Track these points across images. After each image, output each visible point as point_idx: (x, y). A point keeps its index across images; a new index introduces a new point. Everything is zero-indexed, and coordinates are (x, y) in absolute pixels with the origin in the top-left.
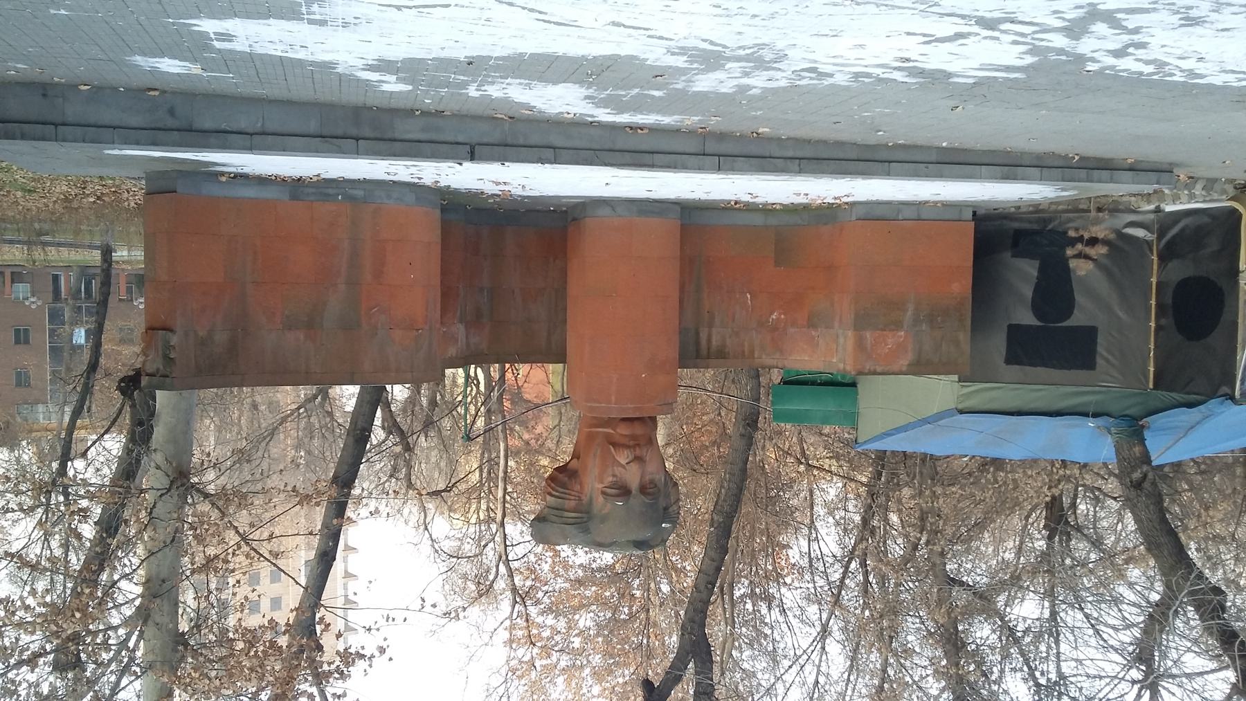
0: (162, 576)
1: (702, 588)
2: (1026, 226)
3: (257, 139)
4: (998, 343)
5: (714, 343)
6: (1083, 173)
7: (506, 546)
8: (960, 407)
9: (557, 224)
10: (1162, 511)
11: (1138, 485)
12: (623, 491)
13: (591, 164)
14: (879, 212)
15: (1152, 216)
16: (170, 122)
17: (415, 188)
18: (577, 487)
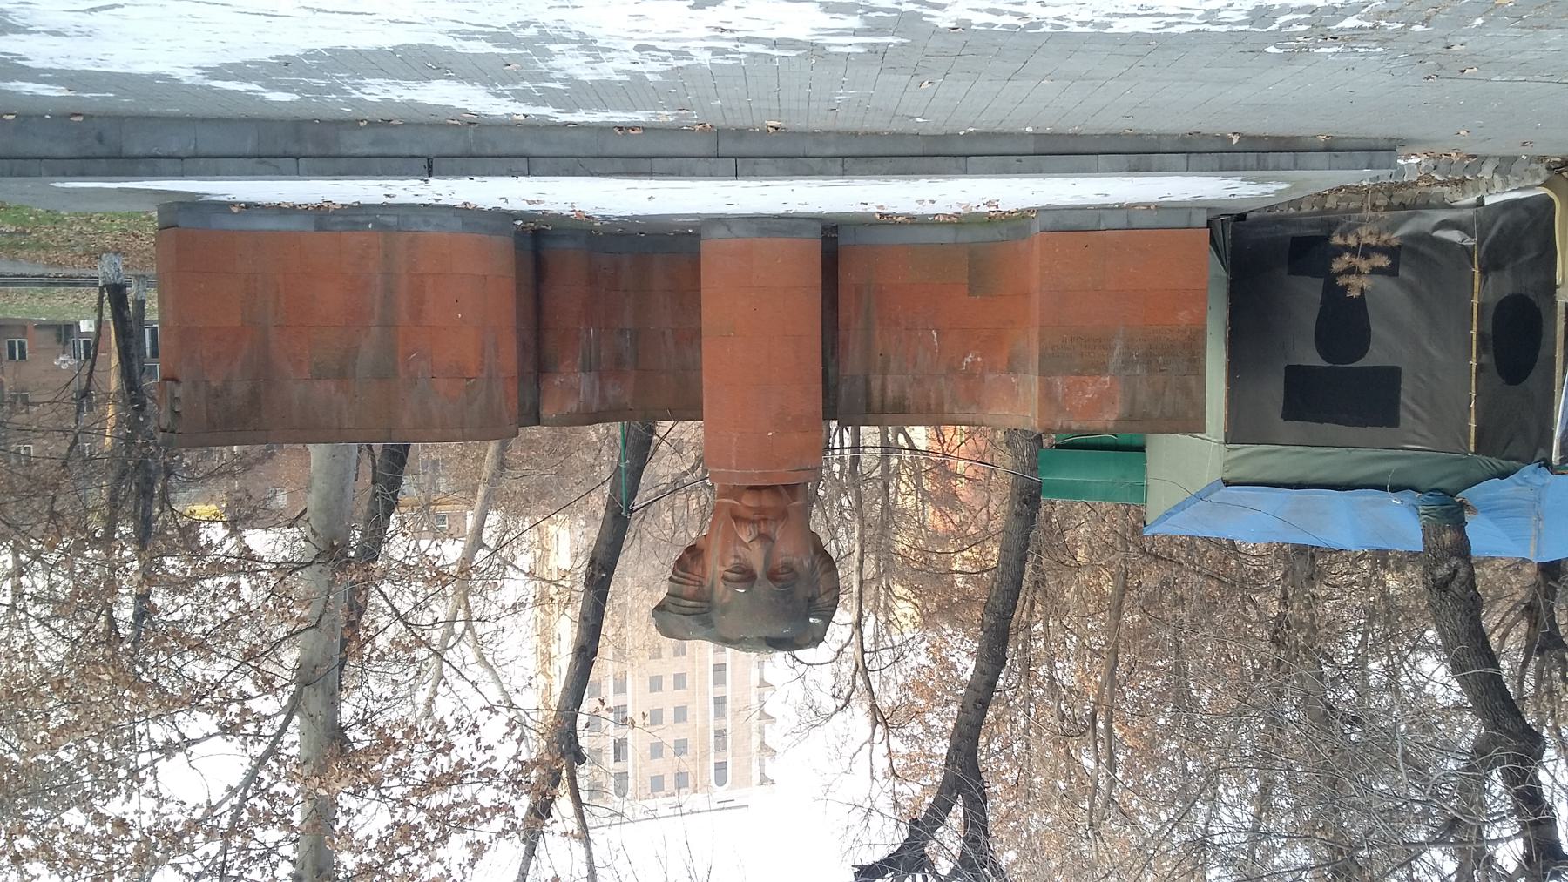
0: (315, 662)
1: (970, 707)
2: (1310, 232)
3: (189, 163)
4: (1274, 391)
5: (890, 394)
6: (1252, 158)
7: (863, 652)
8: (1227, 476)
9: (670, 248)
10: (1476, 620)
11: (1443, 586)
12: (746, 575)
13: (574, 175)
14: (1071, 221)
15: (1470, 212)
16: (100, 150)
17: (466, 214)
18: (699, 571)
